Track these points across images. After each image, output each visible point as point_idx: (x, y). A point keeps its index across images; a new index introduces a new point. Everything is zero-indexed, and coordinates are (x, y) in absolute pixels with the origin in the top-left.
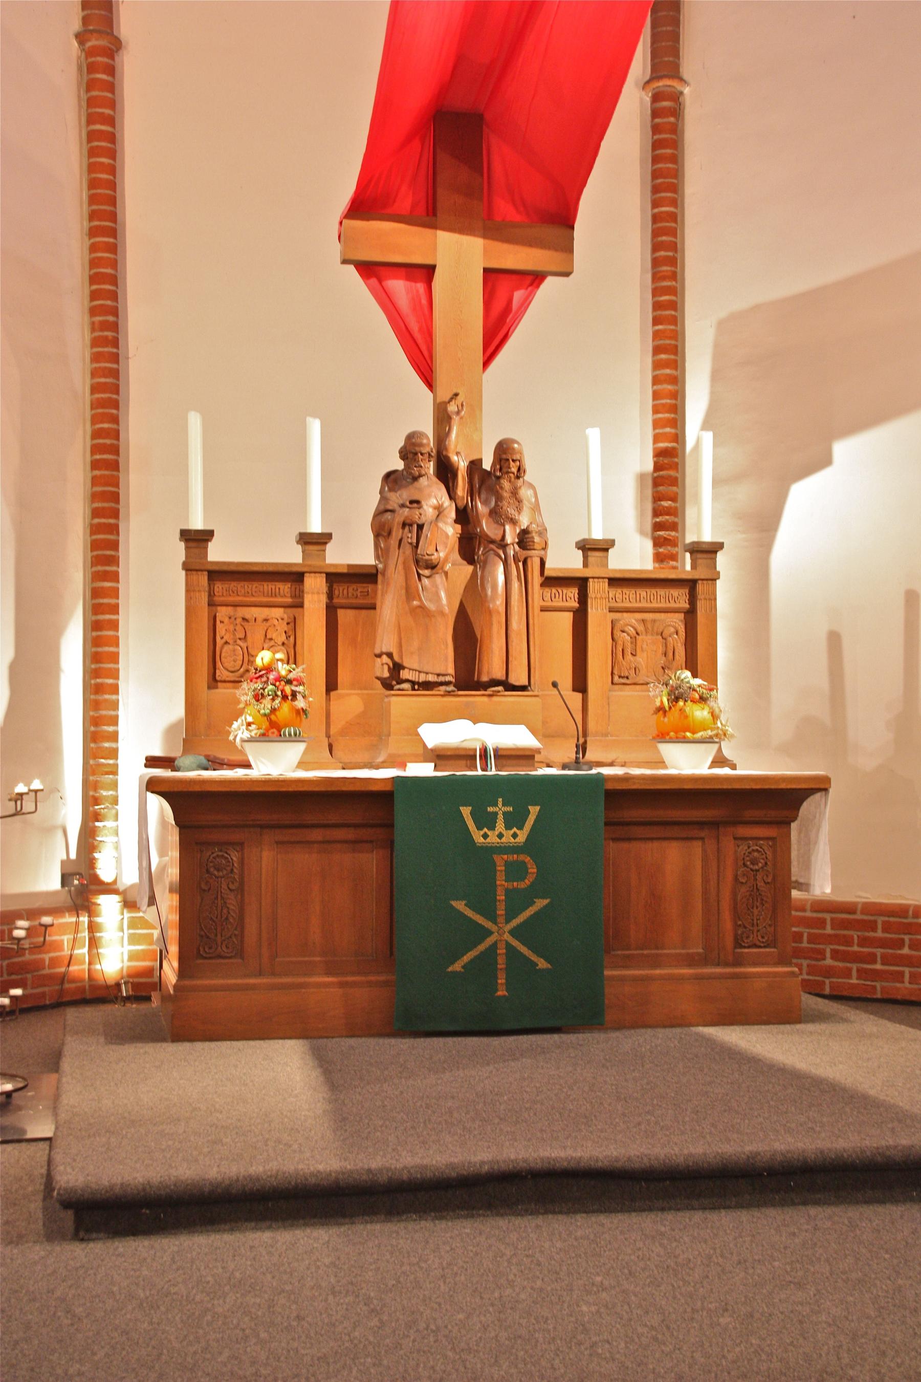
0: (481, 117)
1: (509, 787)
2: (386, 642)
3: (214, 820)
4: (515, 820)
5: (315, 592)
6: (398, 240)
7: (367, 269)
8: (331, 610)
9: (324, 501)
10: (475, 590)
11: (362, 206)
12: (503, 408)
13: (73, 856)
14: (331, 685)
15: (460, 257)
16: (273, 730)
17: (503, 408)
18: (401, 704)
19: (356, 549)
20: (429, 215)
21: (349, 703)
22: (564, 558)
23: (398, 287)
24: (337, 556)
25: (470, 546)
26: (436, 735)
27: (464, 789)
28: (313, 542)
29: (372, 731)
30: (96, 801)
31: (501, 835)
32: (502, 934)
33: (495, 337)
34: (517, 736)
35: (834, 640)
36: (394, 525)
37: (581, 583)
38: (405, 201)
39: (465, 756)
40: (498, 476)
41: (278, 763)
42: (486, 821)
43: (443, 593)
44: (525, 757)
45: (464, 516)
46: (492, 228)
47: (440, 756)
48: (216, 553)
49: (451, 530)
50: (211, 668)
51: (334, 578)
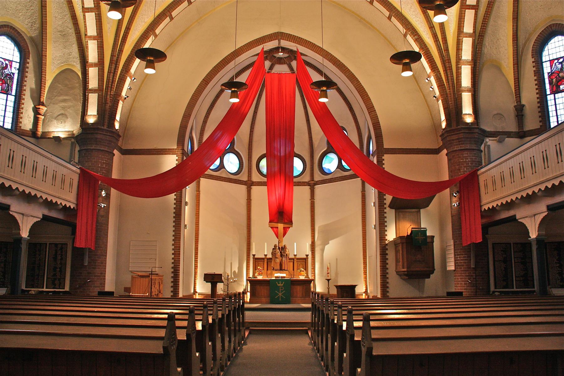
0: (283, 212)
1: (282, 280)
2: (272, 266)
3: (253, 283)
4: (282, 283)
5: (266, 260)
6: (275, 225)
7: (271, 228)
8: (267, 262)
9: (267, 252)
10: (282, 260)
11: (270, 222)
12: (285, 241)
13: (11, 213)
14: (267, 270)
15: (281, 226)
16: (259, 274)
17: (285, 241)
18: (274, 272)
19: (270, 256)
20: (278, 222)
21: (269, 272)
22: (291, 256)
23: (275, 229)
24: (268, 257)
25: (281, 256)
26: (276, 275)
27: (278, 280)
28: (266, 255)
29: (272, 275)
30: (462, 14)
31: (280, 285)
32: (280, 294)
33: (285, 234)
34: (284, 275)
35: (337, 259)
36: (274, 254)
37: (294, 259)
38: (275, 221)
39: (278, 277)
40: (283, 249)
41: (260, 278)
42: (279, 283)
43: (278, 261)
44: (284, 277)
45: (281, 252)
46: (284, 223)
47: (276, 277)
48: (256, 257)
49: (279, 254)
50: (255, 268)
51: (268, 259)
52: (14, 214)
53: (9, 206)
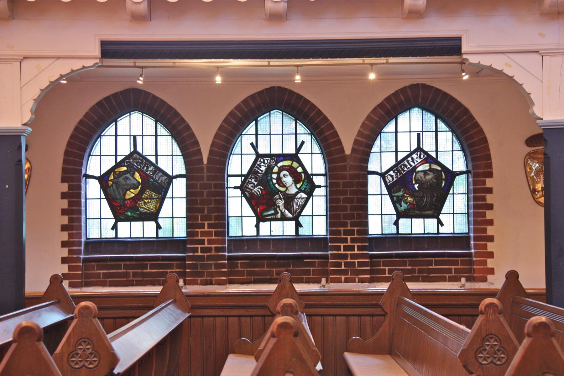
52: (485, 61)
53: (459, 39)
